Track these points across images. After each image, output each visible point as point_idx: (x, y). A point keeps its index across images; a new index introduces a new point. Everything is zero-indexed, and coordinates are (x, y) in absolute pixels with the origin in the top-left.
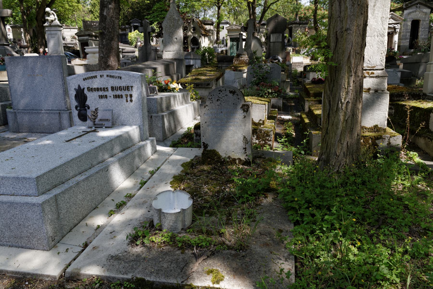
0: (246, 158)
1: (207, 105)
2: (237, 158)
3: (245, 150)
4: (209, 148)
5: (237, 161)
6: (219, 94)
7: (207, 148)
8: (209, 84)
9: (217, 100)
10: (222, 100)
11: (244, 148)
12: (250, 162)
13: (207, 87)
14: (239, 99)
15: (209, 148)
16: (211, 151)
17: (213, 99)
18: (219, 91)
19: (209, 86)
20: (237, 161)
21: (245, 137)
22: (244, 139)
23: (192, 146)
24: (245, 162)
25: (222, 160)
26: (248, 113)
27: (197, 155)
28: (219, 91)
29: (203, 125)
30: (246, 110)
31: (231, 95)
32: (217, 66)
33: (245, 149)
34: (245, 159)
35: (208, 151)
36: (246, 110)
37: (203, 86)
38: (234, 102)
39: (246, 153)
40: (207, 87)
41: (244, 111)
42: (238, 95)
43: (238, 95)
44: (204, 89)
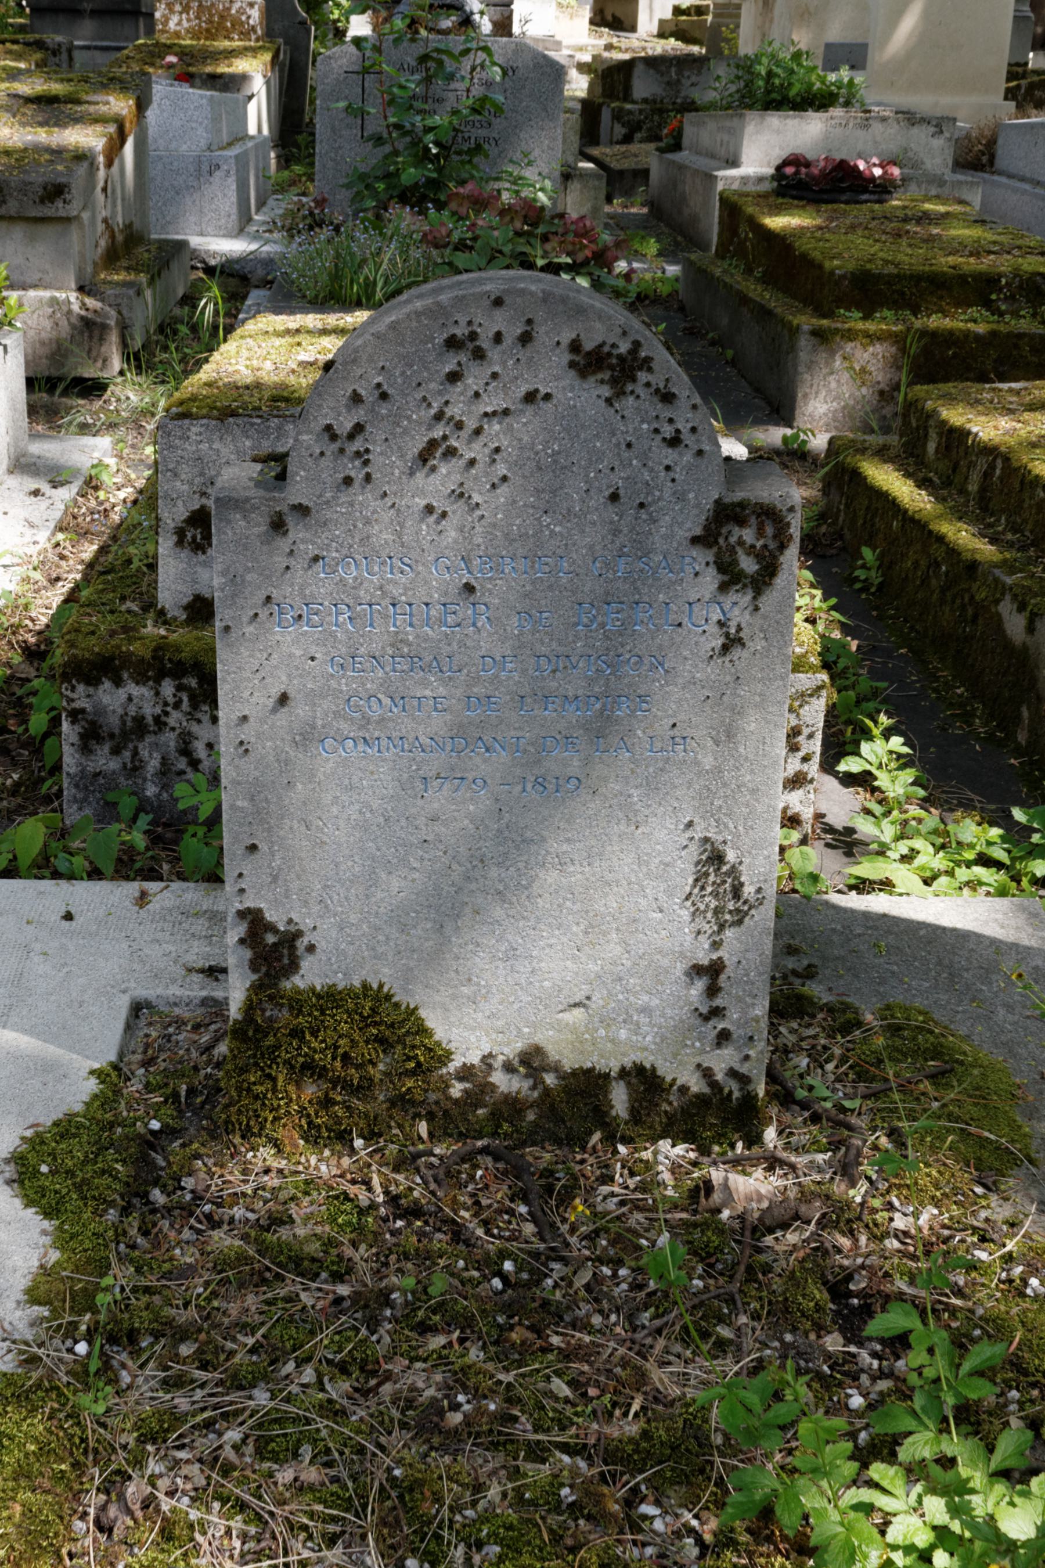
0: (721, 1061)
1: (302, 510)
2: (613, 1065)
3: (712, 991)
4: (310, 975)
5: (619, 1099)
6: (454, 377)
7: (294, 966)
8: (56, 192)
9: (424, 457)
10: (476, 450)
11: (697, 970)
12: (749, 1100)
13: (48, 211)
14: (674, 441)
15: (310, 975)
16: (330, 998)
17: (375, 442)
18: (453, 343)
19: (58, 208)
20: (619, 1099)
21: (717, 858)
22: (700, 879)
23: (61, 863)
24: (701, 1100)
25: (457, 1090)
26: (769, 600)
27: (143, 993)
28: (453, 343)
29: (247, 733)
30: (748, 565)
31: (589, 396)
32: (39, 45)
33: (711, 973)
34: (707, 1073)
35: (297, 1003)
36: (748, 565)
37: (12, 207)
38: (618, 480)
39: (716, 1012)
40: (48, 211)
41: (730, 577)
42: (667, 398)
43: (667, 398)
44: (18, 231)
